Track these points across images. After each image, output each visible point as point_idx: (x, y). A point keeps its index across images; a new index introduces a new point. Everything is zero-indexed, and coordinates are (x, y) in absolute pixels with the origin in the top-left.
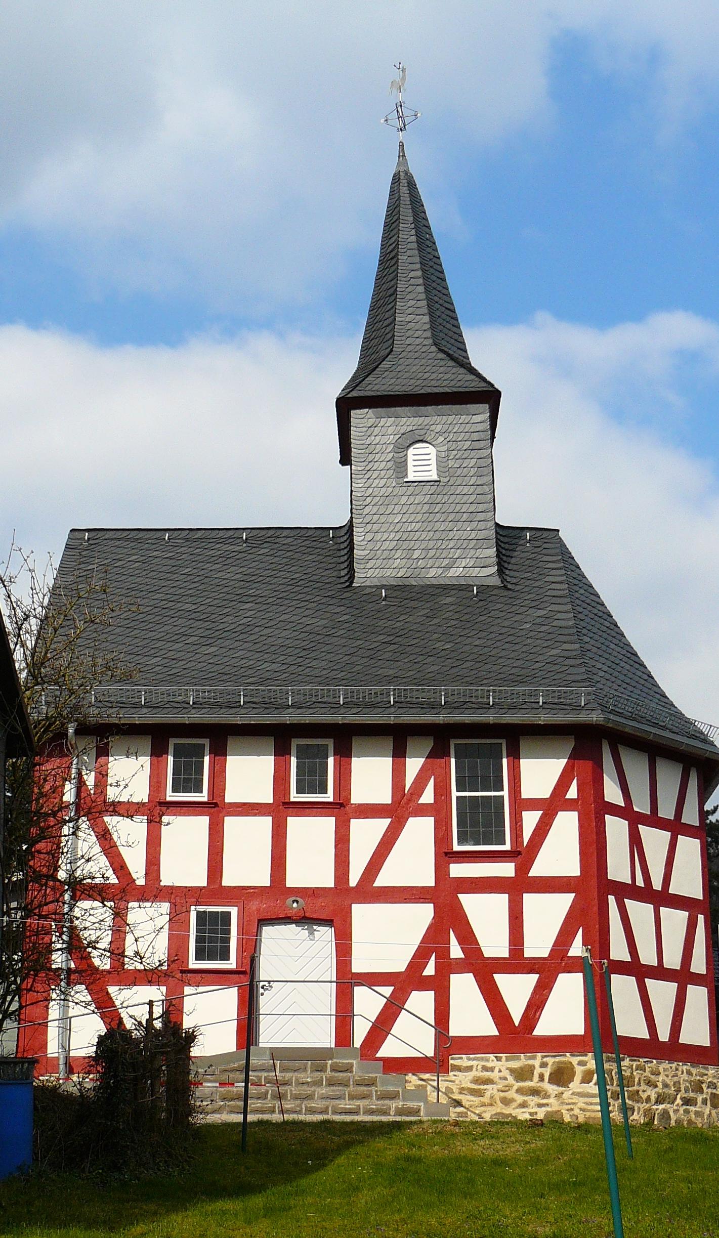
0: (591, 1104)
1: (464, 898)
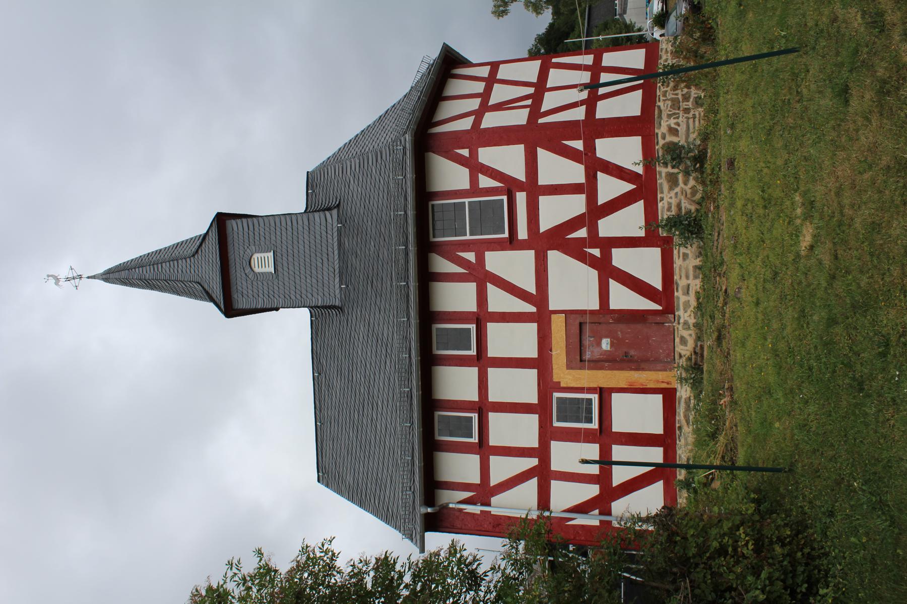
1: (543, 229)
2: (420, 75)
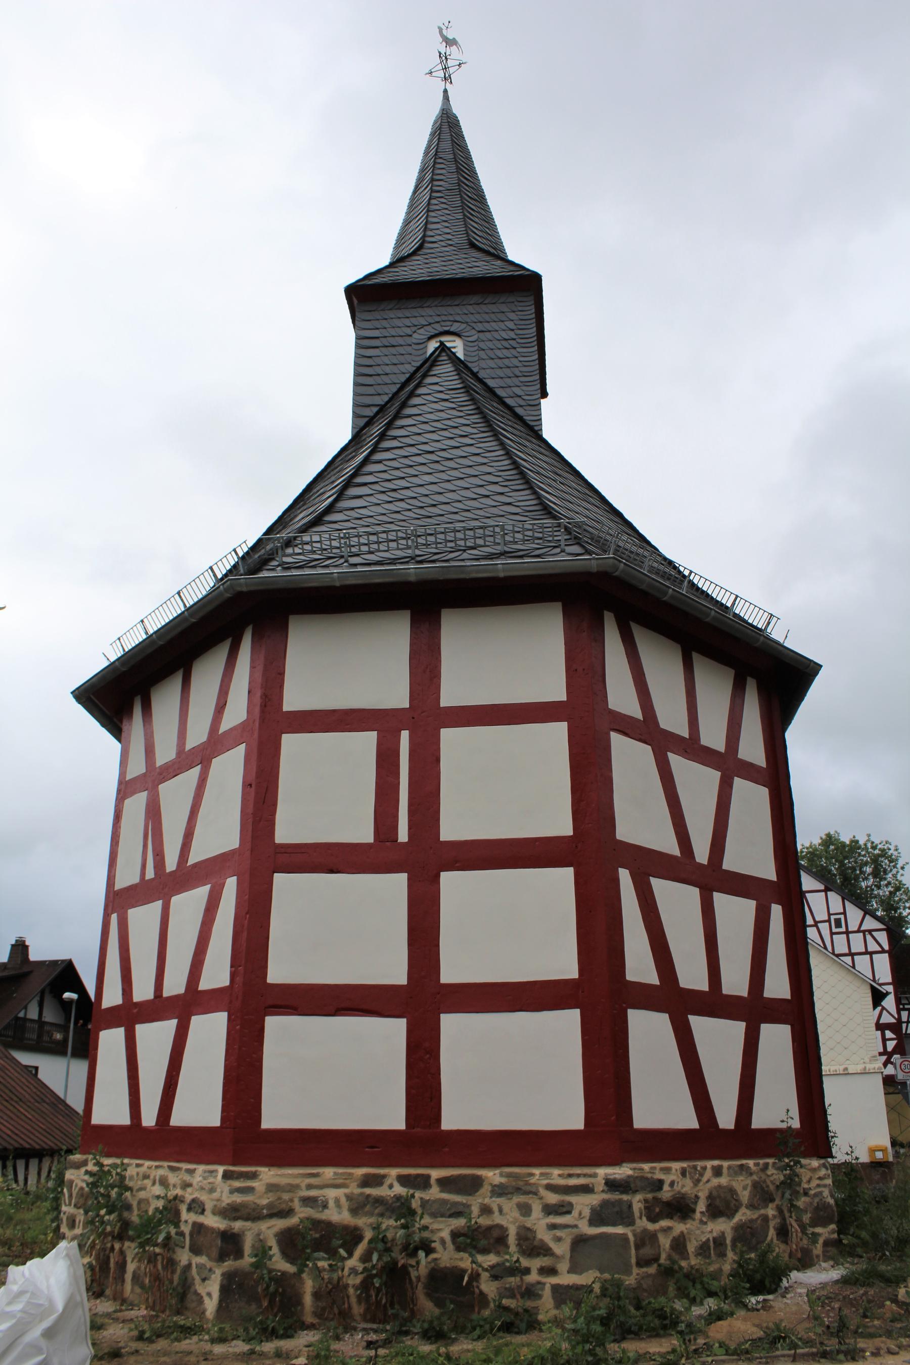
2: (727, 601)
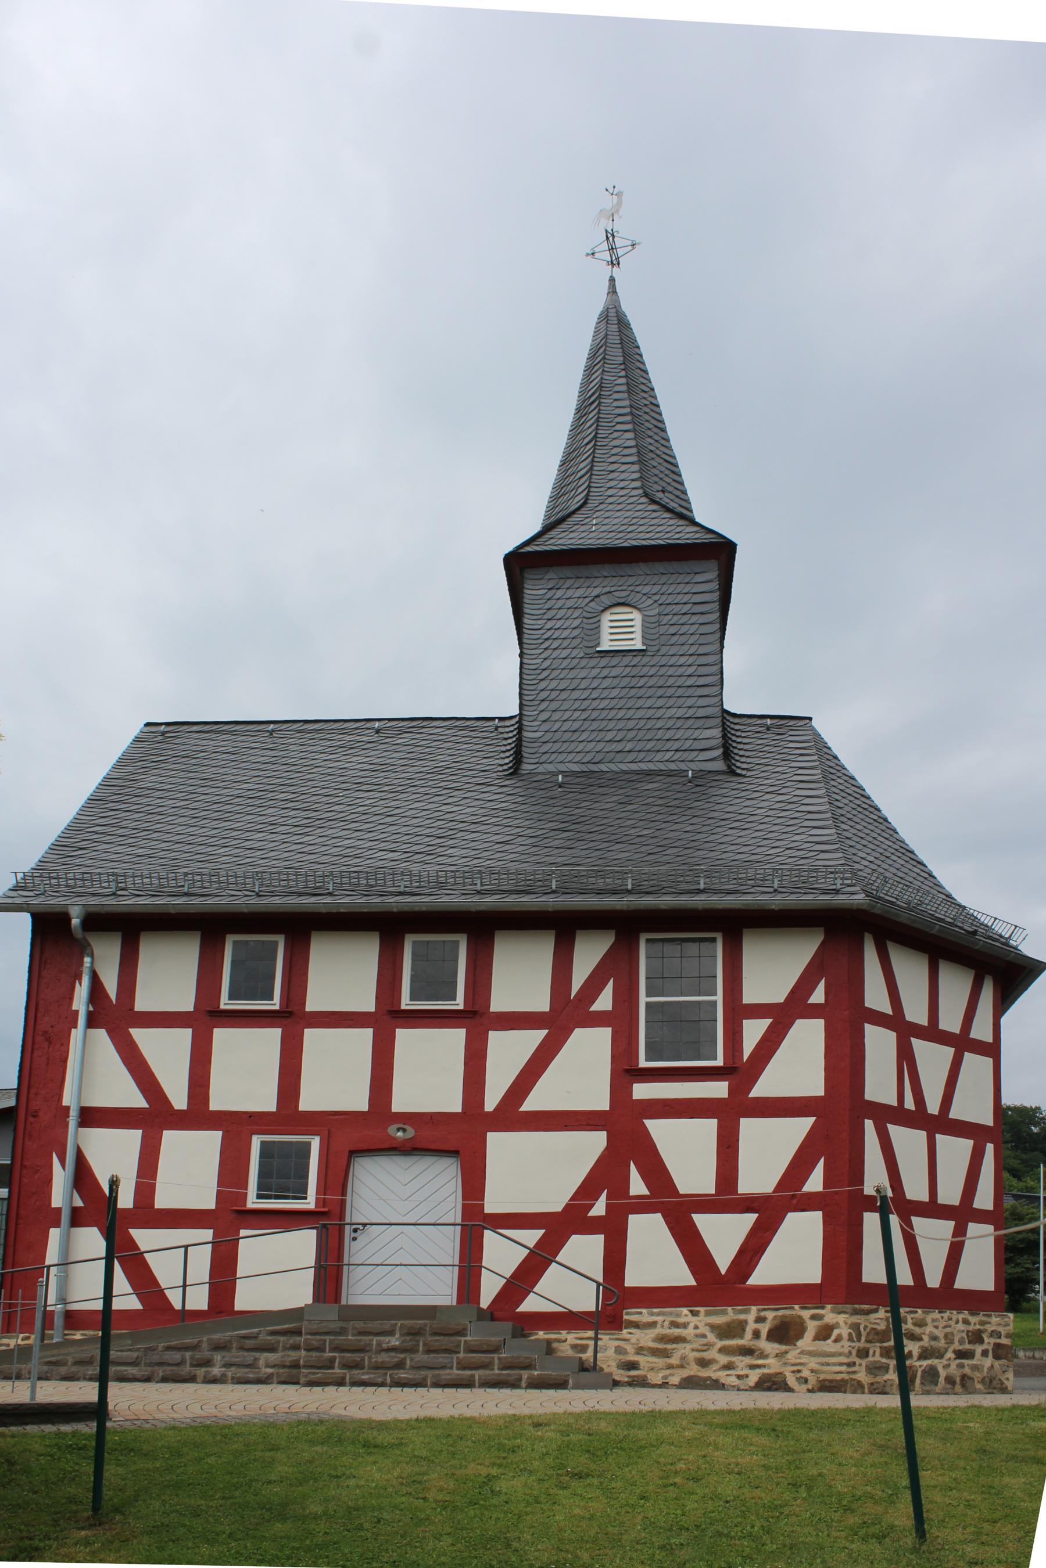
0: (828, 1364)
1: (651, 1124)
